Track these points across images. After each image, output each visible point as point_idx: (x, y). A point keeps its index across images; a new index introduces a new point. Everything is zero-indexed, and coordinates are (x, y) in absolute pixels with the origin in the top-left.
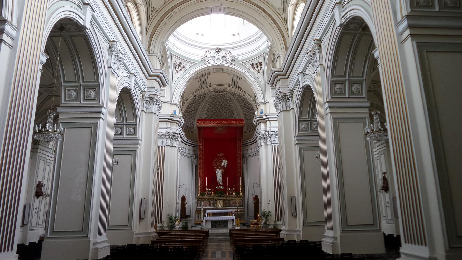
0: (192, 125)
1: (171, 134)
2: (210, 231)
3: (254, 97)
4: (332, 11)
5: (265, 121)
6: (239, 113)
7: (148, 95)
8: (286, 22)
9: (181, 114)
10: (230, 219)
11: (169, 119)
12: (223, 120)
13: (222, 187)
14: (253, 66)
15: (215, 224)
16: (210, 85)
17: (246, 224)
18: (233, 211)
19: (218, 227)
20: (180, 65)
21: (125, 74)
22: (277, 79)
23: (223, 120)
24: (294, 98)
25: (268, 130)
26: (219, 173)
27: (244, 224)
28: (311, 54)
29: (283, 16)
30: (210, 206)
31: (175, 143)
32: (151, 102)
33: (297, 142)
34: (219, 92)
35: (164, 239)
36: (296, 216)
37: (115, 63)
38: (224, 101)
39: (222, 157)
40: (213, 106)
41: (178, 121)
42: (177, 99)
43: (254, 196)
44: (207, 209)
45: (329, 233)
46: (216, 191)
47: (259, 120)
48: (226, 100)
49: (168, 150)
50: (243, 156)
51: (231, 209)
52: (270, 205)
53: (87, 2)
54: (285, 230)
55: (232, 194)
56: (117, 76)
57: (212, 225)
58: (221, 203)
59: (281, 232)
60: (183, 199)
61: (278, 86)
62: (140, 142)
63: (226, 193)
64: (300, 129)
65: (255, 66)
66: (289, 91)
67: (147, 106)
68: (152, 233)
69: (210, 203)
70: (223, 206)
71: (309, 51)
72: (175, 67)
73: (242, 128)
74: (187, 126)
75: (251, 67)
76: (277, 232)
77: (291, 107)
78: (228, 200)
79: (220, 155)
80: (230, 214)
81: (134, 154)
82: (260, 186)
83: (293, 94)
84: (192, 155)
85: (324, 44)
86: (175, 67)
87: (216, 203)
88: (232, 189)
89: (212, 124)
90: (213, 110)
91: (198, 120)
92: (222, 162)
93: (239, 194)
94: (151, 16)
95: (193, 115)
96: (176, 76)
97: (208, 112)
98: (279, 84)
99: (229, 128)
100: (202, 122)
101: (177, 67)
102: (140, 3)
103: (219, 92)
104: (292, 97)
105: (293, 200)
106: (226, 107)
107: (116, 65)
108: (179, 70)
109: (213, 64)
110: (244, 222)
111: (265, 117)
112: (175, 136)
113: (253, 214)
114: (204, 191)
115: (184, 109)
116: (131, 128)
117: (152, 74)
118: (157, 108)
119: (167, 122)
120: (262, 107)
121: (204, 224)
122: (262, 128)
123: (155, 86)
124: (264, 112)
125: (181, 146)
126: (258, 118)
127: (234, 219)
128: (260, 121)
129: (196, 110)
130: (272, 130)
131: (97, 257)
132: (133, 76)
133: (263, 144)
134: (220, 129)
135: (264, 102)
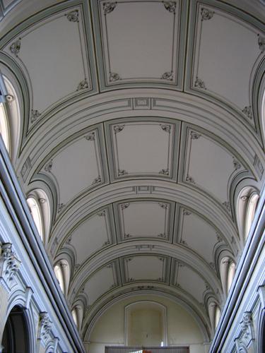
8: (234, 218)
21: (20, 287)
24: (254, 324)
29: (252, 122)
37: (7, 272)
56: (8, 290)
85: (255, 317)
94: (58, 215)
102: (12, 94)
107: (8, 276)
132: (57, 340)
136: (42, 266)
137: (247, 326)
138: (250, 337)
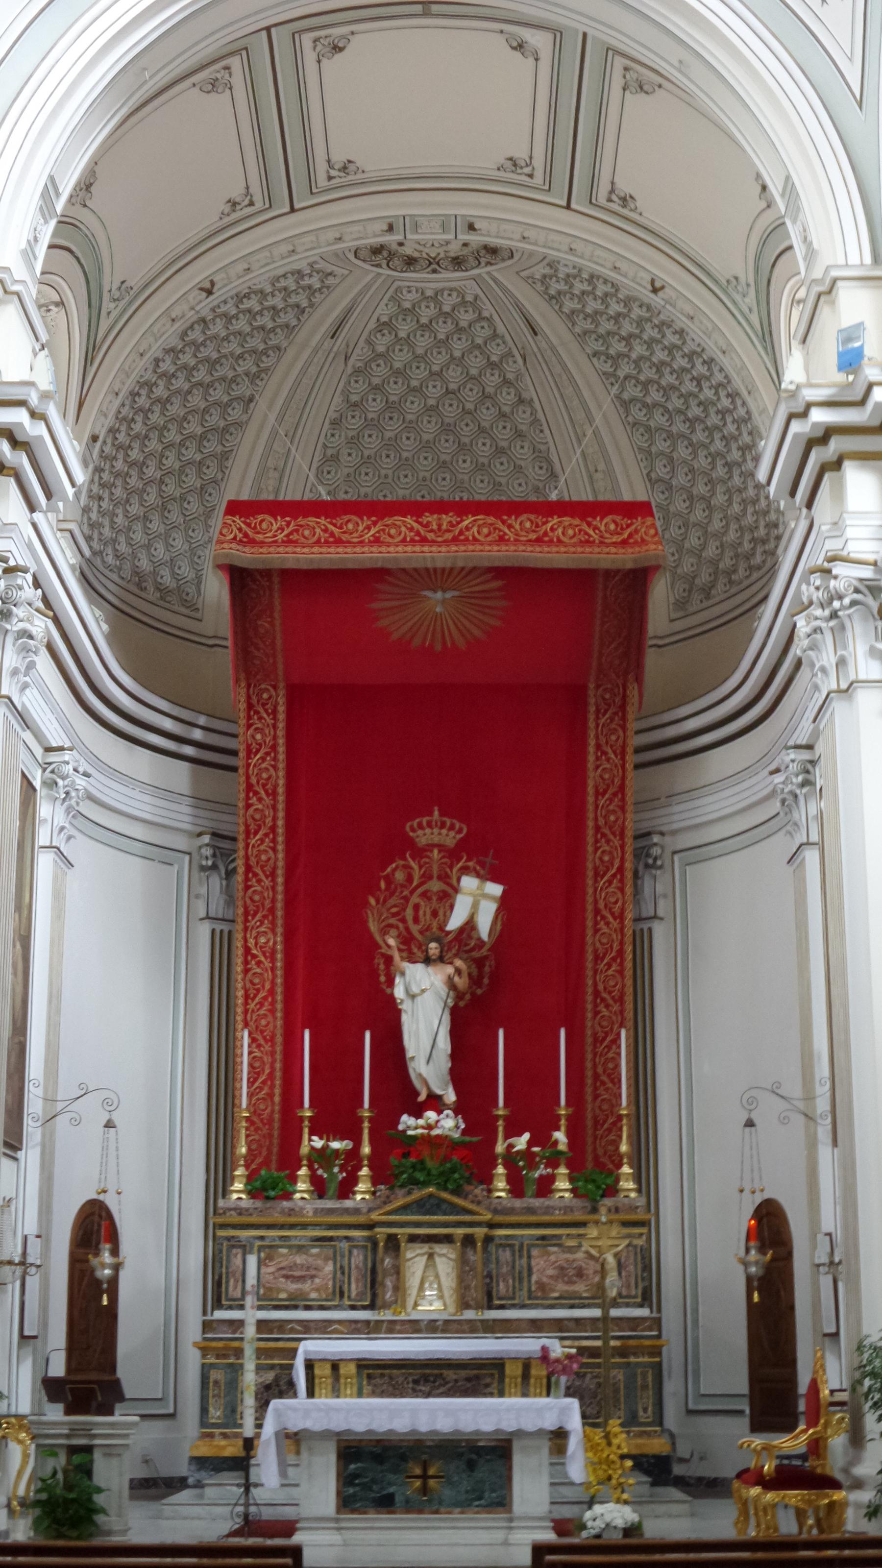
0: (185, 570)
4: (814, 721)
10: (530, 1425)
12: (463, 508)
13: (448, 1124)
15: (374, 1474)
17: (678, 1470)
18: (557, 1349)
19: (410, 1507)
23: (463, 508)
26: (424, 1000)
27: (657, 1470)
30: (339, 1295)
34: (434, 264)
39: (453, 854)
40: (374, 407)
44: (309, 1328)
46: (396, 1160)
47: (827, 434)
48: (496, 352)
50: (641, 853)
51: (536, 1326)
53: (54, 745)
55: (545, 1187)
57: (346, 1479)
58: (446, 1261)
60: (95, 1227)
63: (487, 1179)
70: (464, 1305)
74: (139, 578)
78: (507, 1244)
79: (435, 833)
80: (533, 1376)
84: (181, 842)
87: (397, 1271)
88: (541, 1138)
89: (359, 548)
90: (372, 444)
91: (235, 508)
92: (447, 898)
93: (612, 1191)
95: (192, 480)
99: (513, 577)
100: (272, 526)
103: (434, 264)
110: (657, 1445)
113: (728, 1369)
114: (289, 1160)
121: (267, 1468)
126: (818, 416)
127: (574, 1423)
134: (437, 600)
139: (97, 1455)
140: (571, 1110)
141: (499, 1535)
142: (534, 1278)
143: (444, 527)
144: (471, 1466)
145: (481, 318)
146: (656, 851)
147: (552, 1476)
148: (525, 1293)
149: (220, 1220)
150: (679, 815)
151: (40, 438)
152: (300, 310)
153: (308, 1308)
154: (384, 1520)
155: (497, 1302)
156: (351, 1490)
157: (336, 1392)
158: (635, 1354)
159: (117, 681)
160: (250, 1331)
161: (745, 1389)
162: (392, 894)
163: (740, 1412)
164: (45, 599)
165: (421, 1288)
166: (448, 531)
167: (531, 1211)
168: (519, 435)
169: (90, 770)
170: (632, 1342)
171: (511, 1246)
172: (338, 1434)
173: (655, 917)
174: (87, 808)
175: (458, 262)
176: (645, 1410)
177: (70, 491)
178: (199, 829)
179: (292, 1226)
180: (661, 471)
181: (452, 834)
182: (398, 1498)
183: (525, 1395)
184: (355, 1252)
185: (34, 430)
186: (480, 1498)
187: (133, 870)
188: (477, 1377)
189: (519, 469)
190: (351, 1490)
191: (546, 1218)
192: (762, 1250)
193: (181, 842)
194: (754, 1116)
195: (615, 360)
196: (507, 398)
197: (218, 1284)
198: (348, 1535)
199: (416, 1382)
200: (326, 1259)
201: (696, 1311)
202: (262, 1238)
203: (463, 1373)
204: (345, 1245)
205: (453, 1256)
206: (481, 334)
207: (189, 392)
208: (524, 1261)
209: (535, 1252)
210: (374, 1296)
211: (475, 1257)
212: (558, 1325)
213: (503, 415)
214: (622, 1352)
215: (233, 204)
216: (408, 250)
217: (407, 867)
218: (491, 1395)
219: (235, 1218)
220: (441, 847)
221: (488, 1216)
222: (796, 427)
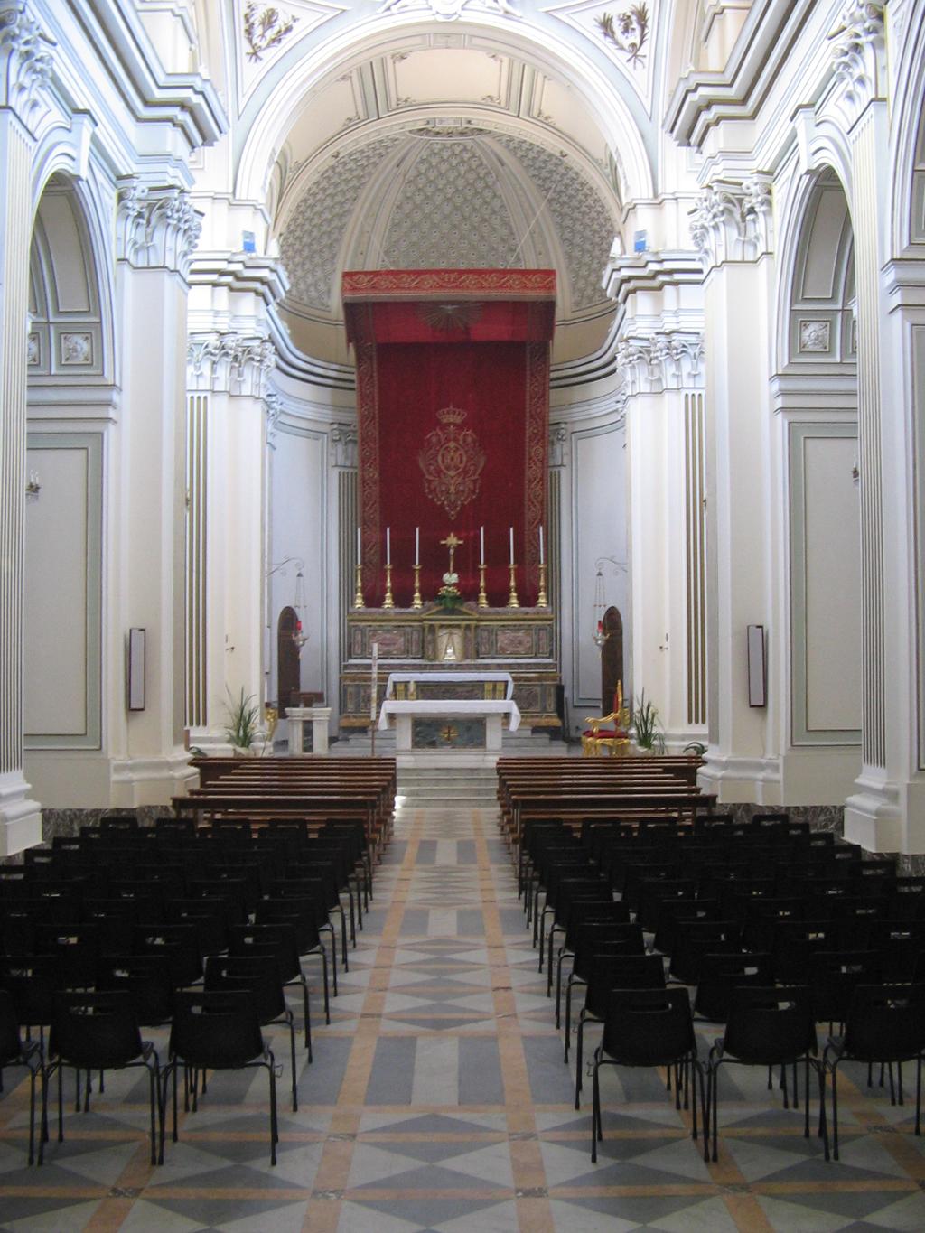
1: (230, 341)
2: (404, 761)
3: (612, 171)
5: (655, 283)
6: (535, 245)
7: (140, 189)
9: (274, 251)
11: (222, 273)
14: (606, 25)
15: (428, 732)
16: (406, 105)
20: (269, 20)
22: (705, 117)
24: (777, 208)
25: (668, 328)
28: (843, 41)
30: (406, 652)
31: (250, 381)
32: (154, 220)
33: (779, 403)
34: (450, 134)
35: (222, 789)
36: (764, 706)
37: (22, 89)
38: (471, 177)
40: (418, 198)
41: (263, 281)
42: (257, 181)
43: (601, 615)
45: (872, 777)
47: (629, 279)
49: (218, 409)
51: (500, 667)
52: (667, 654)
53: (81, 107)
54: (716, 763)
57: (415, 734)
58: (457, 638)
59: (701, 769)
60: (289, 621)
61: (711, 145)
62: (115, 397)
63: (477, 599)
64: (796, 346)
65: (617, 26)
66: (756, 178)
67: (141, 240)
68: (179, 764)
69: (409, 641)
70: (466, 656)
71: (835, 29)
72: (249, 32)
73: (550, 306)
75: (599, 32)
76: (687, 768)
77: (761, 248)
78: (486, 628)
80: (497, 690)
81: (91, 445)
82: (624, 568)
83: (775, 189)
84: (326, 428)
86: (249, 32)
87: (434, 642)
90: (417, 217)
96: (252, 72)
97: (396, 225)
98: (718, 139)
101: (258, 30)
104: (768, 203)
105: (755, 642)
106: (478, 202)
107: (25, 96)
108: (263, 44)
109: (426, 16)
111: (655, 267)
112: (247, 350)
113: (592, 686)
115: (285, 216)
116: (79, 339)
117: (159, 95)
118: (182, 245)
119: (215, 285)
120: (643, 220)
122: (640, 318)
123: (169, 149)
124: (651, 243)
125: (275, 385)
126: (625, 273)
128: (632, 285)
129: (341, 216)
130: (684, 327)
131: (5, 848)
132: (86, 120)
133: (645, 388)
135: (656, 196)
136: (122, 49)
137: (857, 48)
138: (866, 93)
139: (315, 725)
140: (516, 566)
141: (480, 758)
142: (499, 645)
143: (452, 280)
144: (469, 729)
145: (474, 156)
146: (563, 432)
147: (503, 734)
148: (494, 651)
149: (351, 618)
150: (577, 413)
151: (199, 104)
152: (381, 155)
153: (392, 658)
154: (432, 751)
155: (481, 656)
156: (418, 739)
157: (406, 698)
158: (546, 680)
159: (296, 356)
160: (375, 669)
161: (601, 697)
162: (431, 448)
163: (598, 707)
164: (276, 349)
165: (446, 650)
166: (453, 282)
167: (498, 613)
168: (494, 212)
169: (284, 400)
170: (544, 675)
171: (488, 630)
172: (412, 714)
173: (562, 465)
174: (283, 418)
175: (462, 134)
176: (550, 706)
177: (283, 294)
178: (331, 421)
179: (384, 621)
180: (568, 235)
181: (459, 417)
182: (438, 742)
183: (494, 699)
184: (414, 633)
185: (272, 277)
186: (472, 742)
187: (302, 443)
188: (472, 691)
189: (494, 229)
190: (418, 739)
191: (504, 617)
192: (604, 634)
193: (326, 428)
194: (602, 571)
195: (545, 180)
196: (488, 194)
197: (350, 647)
198: (417, 757)
199: (444, 692)
200: (401, 636)
201: (578, 658)
202: (370, 626)
203: (465, 689)
204: (409, 629)
205: (460, 634)
206: (474, 164)
207: (324, 200)
208: (494, 637)
209: (499, 633)
210: (423, 653)
211: (471, 635)
212: (509, 666)
213: (486, 203)
214: (539, 679)
215: (350, 120)
216: (437, 130)
217: (437, 435)
218: (478, 699)
219: (356, 617)
220: (455, 424)
221: (477, 616)
222: (616, 275)
